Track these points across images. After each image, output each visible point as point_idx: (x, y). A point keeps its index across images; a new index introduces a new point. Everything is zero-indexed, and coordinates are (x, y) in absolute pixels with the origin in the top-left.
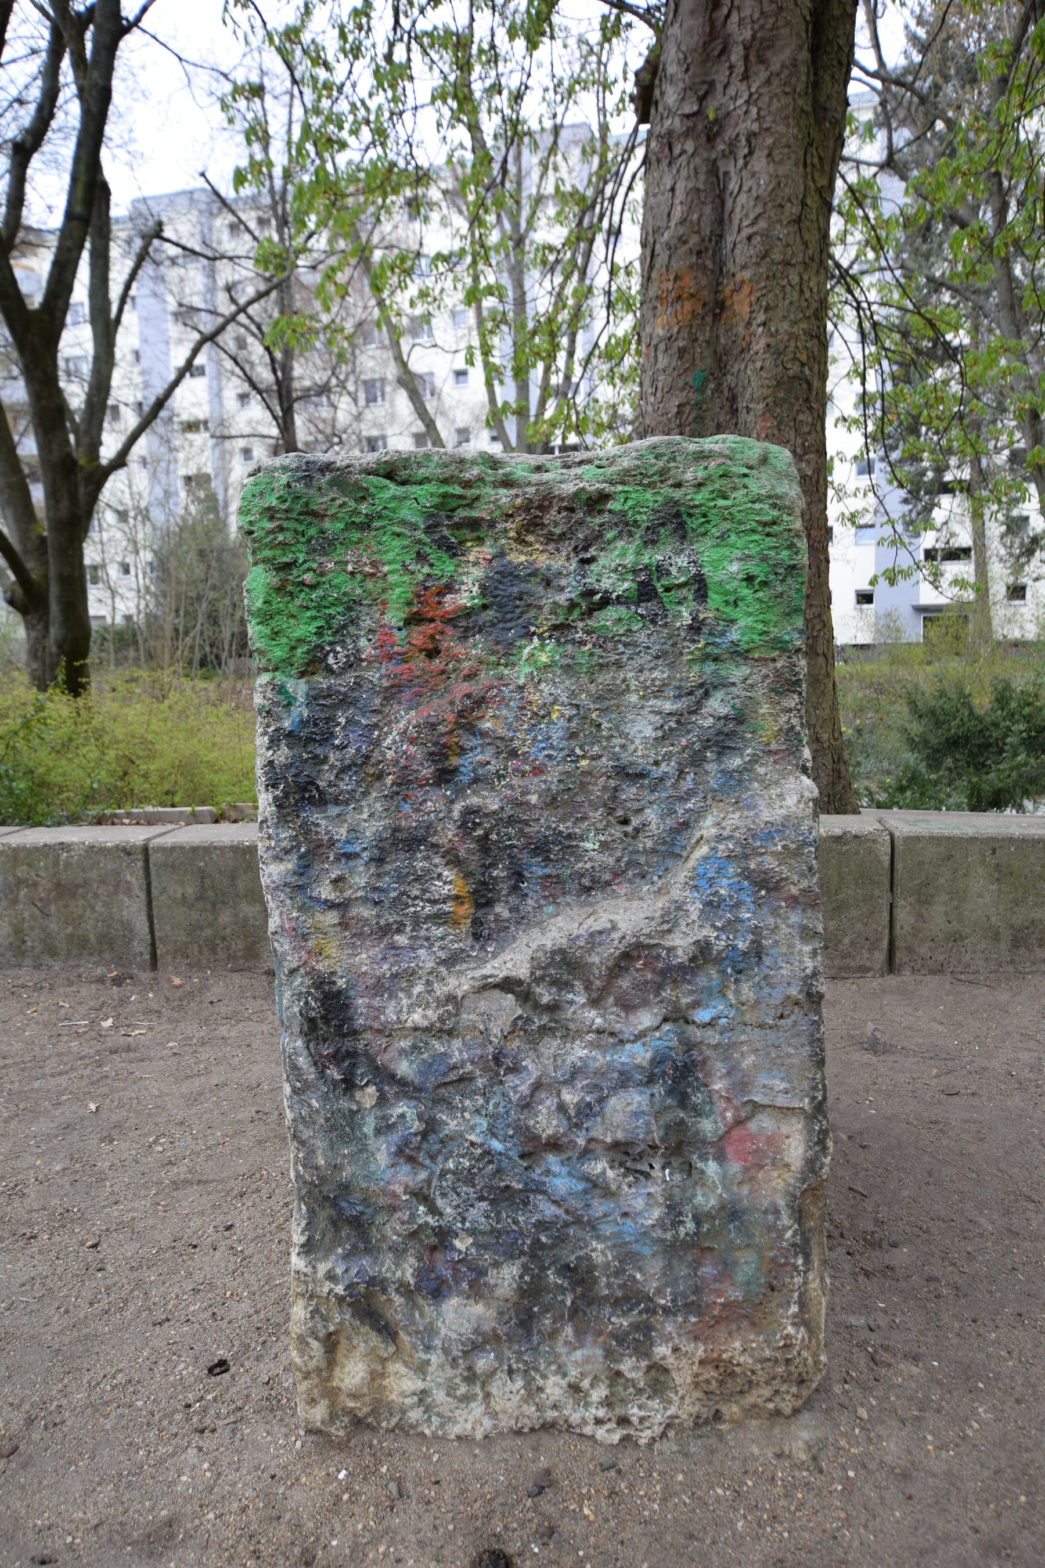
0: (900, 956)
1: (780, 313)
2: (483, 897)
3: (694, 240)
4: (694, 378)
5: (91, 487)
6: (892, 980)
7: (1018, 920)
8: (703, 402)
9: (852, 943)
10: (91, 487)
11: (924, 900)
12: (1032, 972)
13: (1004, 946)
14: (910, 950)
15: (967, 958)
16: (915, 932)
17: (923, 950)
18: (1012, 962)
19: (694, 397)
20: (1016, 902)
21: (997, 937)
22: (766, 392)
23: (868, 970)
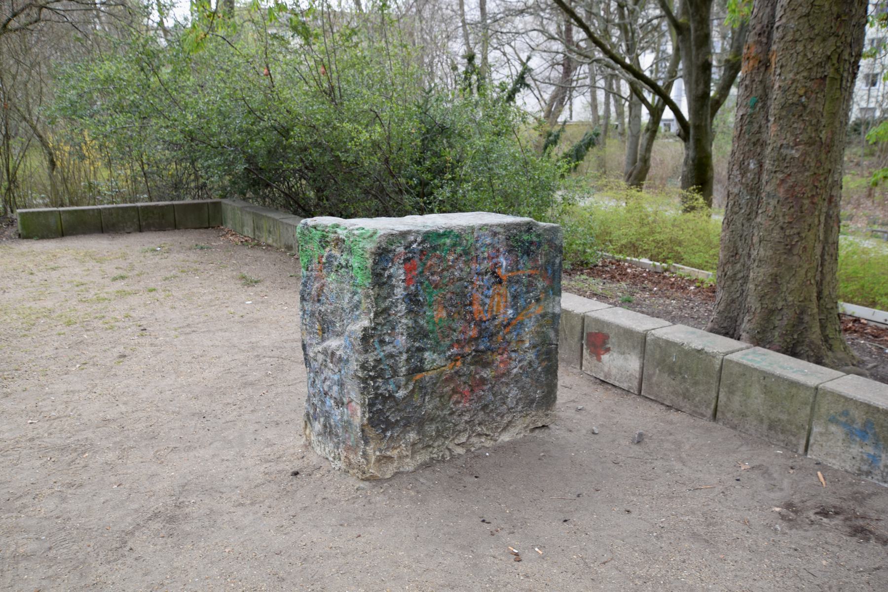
0: (719, 414)
1: (788, 69)
2: (323, 331)
3: (759, 27)
4: (752, 100)
5: (732, 72)
6: (712, 424)
7: (773, 416)
8: (754, 114)
9: (699, 401)
10: (732, 72)
11: (731, 392)
12: (776, 445)
13: (765, 427)
14: (723, 413)
15: (747, 426)
16: (726, 406)
17: (729, 415)
18: (767, 436)
19: (750, 111)
20: (772, 407)
21: (762, 421)
22: (776, 112)
23: (704, 416)
